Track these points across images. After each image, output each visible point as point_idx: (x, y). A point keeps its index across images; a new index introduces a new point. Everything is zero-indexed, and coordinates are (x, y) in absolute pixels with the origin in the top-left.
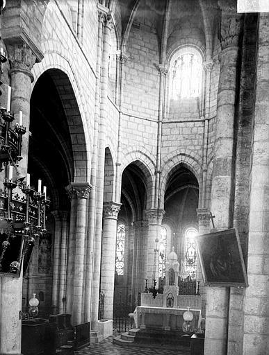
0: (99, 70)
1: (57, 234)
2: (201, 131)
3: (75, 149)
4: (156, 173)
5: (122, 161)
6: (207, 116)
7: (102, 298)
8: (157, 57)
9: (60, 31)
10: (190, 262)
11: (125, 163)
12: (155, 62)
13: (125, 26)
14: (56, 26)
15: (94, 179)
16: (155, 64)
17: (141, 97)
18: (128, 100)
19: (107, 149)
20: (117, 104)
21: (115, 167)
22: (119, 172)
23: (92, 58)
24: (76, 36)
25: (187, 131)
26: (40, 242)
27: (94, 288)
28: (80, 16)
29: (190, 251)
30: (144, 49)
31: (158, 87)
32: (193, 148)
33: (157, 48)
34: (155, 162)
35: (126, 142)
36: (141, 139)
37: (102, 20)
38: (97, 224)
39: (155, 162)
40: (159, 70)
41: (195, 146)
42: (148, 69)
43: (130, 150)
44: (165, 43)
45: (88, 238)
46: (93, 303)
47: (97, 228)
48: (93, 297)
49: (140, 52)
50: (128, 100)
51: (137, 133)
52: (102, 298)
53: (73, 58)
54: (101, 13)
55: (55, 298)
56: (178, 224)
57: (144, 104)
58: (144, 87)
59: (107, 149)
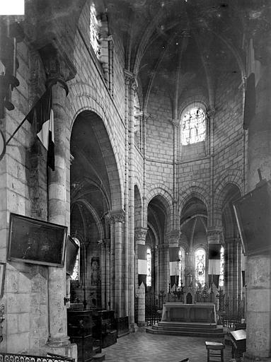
0: (127, 122)
1: (102, 257)
2: (207, 166)
3: (112, 185)
4: (173, 203)
5: (147, 195)
6: (212, 153)
7: (137, 299)
8: (171, 115)
9: (95, 81)
10: (200, 273)
11: (150, 197)
12: (168, 118)
13: (144, 93)
14: (91, 75)
15: (127, 206)
16: (169, 121)
17: (160, 150)
18: (149, 149)
19: (136, 186)
20: (142, 152)
21: (142, 200)
22: (145, 204)
23: (121, 111)
24: (111, 97)
25: (196, 168)
26: (92, 263)
27: (130, 290)
28: (111, 75)
29: (199, 265)
30: (161, 109)
31: (172, 136)
32: (201, 180)
33: (170, 108)
34: (172, 195)
35: (149, 181)
36: (160, 178)
37: (128, 83)
38: (131, 241)
39: (172, 195)
40: (173, 125)
41: (203, 178)
42: (164, 125)
43: (153, 187)
44: (177, 102)
45: (124, 252)
46: (130, 302)
47: (131, 223)
48: (130, 297)
49: (158, 112)
50: (149, 149)
51: (158, 174)
52: (137, 299)
53: (107, 107)
54: (127, 77)
55: (103, 303)
56: (137, 338)
57: (162, 152)
58: (161, 139)
59: (136, 186)
